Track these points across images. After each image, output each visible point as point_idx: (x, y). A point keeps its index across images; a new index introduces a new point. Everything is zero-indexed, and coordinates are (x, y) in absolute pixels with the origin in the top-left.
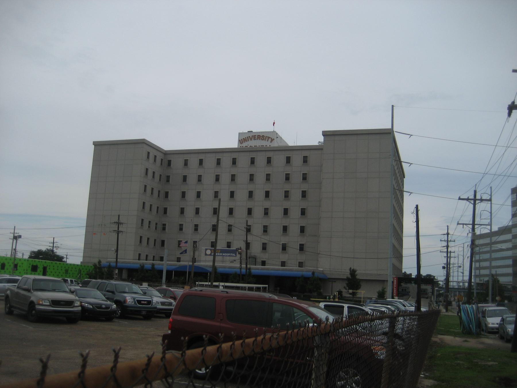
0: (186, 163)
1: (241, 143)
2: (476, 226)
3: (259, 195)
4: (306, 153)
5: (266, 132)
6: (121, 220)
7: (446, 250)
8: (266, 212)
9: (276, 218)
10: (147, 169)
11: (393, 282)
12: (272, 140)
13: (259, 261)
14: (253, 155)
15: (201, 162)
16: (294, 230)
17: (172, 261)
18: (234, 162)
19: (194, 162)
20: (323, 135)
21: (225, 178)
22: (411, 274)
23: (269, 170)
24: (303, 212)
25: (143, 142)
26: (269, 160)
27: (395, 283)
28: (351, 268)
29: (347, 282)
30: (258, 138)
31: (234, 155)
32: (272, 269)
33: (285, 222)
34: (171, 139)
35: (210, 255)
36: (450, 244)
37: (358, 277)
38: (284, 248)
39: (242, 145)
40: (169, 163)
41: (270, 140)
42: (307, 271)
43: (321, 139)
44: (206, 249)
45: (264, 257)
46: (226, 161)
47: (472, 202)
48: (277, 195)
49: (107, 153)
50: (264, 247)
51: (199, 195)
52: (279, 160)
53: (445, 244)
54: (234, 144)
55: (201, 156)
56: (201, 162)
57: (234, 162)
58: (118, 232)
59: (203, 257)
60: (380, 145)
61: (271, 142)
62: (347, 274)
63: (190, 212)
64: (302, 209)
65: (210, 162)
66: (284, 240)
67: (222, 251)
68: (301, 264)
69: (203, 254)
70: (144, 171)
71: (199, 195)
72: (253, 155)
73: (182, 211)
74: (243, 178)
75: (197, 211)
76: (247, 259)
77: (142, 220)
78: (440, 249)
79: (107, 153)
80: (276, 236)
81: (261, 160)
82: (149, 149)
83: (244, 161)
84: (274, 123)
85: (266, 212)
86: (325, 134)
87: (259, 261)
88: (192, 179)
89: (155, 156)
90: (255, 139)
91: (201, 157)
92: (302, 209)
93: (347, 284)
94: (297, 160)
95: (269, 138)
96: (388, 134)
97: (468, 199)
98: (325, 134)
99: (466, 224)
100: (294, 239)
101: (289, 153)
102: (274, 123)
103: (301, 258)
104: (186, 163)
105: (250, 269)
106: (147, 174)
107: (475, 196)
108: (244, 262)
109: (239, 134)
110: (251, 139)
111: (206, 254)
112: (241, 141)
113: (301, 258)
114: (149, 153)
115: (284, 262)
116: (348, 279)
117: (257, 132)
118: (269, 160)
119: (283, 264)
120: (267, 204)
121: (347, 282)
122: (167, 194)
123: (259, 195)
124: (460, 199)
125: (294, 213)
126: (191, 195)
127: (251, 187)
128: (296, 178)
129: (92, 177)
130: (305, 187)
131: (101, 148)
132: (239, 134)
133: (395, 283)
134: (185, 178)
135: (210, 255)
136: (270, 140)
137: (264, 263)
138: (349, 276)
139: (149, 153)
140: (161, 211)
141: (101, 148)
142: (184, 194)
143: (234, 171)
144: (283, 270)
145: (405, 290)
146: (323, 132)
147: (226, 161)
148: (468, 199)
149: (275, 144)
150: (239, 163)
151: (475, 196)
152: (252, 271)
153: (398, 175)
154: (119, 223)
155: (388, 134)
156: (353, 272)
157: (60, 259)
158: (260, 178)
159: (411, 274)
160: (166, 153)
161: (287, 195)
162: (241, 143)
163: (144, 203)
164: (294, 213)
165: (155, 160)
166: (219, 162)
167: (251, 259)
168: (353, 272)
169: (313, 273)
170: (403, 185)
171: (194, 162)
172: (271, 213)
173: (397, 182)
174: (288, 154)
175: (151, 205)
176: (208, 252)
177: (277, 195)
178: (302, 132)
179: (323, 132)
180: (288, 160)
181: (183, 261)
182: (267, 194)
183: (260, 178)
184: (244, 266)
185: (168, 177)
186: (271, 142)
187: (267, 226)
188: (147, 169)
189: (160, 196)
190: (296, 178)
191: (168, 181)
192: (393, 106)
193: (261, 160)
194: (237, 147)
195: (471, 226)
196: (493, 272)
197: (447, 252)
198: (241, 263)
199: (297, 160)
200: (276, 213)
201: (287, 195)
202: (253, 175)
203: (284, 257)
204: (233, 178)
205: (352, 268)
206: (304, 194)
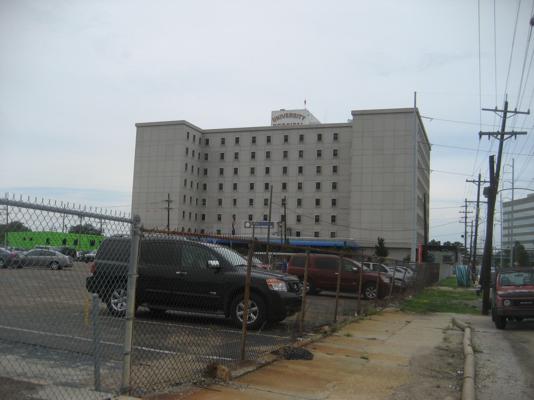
0: (223, 142)
1: (274, 121)
2: (480, 204)
3: (293, 170)
4: (336, 131)
5: (298, 110)
6: (172, 198)
7: (464, 221)
8: (300, 186)
9: (309, 193)
10: (187, 149)
11: (417, 250)
12: (304, 118)
13: (294, 232)
14: (286, 133)
15: (237, 140)
16: (326, 203)
17: (310, 236)
18: (269, 140)
19: (230, 140)
20: (353, 115)
21: (261, 155)
22: (439, 242)
23: (301, 147)
24: (334, 186)
25: (183, 124)
26: (302, 138)
27: (420, 251)
28: (379, 238)
29: (376, 250)
30: (290, 116)
31: (269, 134)
32: (308, 240)
33: (318, 196)
34: (209, 118)
35: (250, 227)
36: (468, 215)
37: (385, 246)
38: (317, 219)
39: (275, 123)
40: (207, 142)
41: (302, 118)
42: (339, 240)
43: (351, 118)
44: (246, 222)
45: (298, 228)
46: (261, 139)
47: (477, 183)
48: (310, 170)
49: (149, 134)
50: (299, 219)
51: (236, 171)
52: (311, 137)
53: (464, 215)
54: (268, 123)
55: (237, 134)
56: (237, 140)
57: (269, 140)
58: (169, 209)
59: (243, 230)
60: (409, 120)
61: (303, 120)
62: (376, 243)
63: (228, 187)
64: (333, 183)
65: (246, 140)
66: (317, 212)
67: (261, 224)
68: (317, 234)
69: (243, 227)
70: (184, 151)
71: (236, 171)
72: (286, 133)
73: (221, 187)
74: (277, 155)
75: (235, 187)
76: (285, 231)
77: (185, 196)
78: (459, 220)
79: (149, 134)
80: (309, 210)
81: (294, 137)
82: (189, 130)
83: (277, 139)
84: (305, 101)
85: (300, 186)
86: (354, 113)
87: (294, 232)
88: (229, 156)
89: (194, 136)
90: (287, 117)
91: (237, 135)
92: (333, 183)
93: (376, 253)
94: (328, 137)
95: (301, 115)
96: (414, 113)
97: (474, 181)
98: (354, 113)
99: (472, 202)
100: (326, 211)
101: (320, 131)
102: (305, 101)
103: (333, 229)
104: (223, 142)
105: (288, 239)
106: (187, 153)
107: (480, 178)
108: (283, 233)
109: (272, 112)
110: (284, 117)
111: (245, 227)
112: (274, 119)
113: (333, 229)
114: (188, 133)
115: (299, 232)
116: (376, 247)
117: (289, 111)
118: (302, 138)
119: (317, 234)
120: (301, 179)
121: (376, 250)
122: (206, 171)
123: (293, 170)
124: (467, 181)
125: (327, 187)
126: (229, 171)
127: (285, 164)
128: (328, 154)
129: (136, 157)
130: (335, 162)
131: (142, 128)
132: (272, 112)
133: (420, 251)
134: (222, 156)
135: (250, 227)
136: (302, 118)
137: (298, 234)
138: (378, 245)
139: (188, 133)
140: (201, 187)
141: (142, 128)
142: (222, 171)
143: (268, 148)
144: (317, 240)
145: (431, 257)
146: (352, 111)
147: (261, 139)
148: (474, 181)
149: (306, 122)
150: (273, 140)
151: (480, 178)
152: (290, 241)
153: (423, 149)
154: (169, 201)
155: (414, 113)
156: (381, 241)
157: (27, 230)
158: (294, 155)
159: (439, 242)
160: (204, 133)
161: (319, 170)
162: (274, 121)
163: (185, 180)
164: (327, 187)
165: (194, 140)
166: (254, 140)
167: (288, 231)
168: (381, 241)
169: (345, 243)
170: (429, 158)
171: (230, 140)
172: (305, 187)
173: (423, 157)
174: (320, 132)
175: (192, 182)
176: (248, 225)
177: (310, 170)
178: (332, 110)
179: (352, 111)
180: (320, 137)
181: (339, 237)
182: (300, 170)
183: (294, 155)
184: (284, 237)
185: (207, 155)
186: (303, 120)
187: (335, 216)
188: (187, 149)
189: (200, 173)
190: (328, 154)
191: (206, 158)
192: (415, 93)
193: (294, 137)
194: (270, 126)
195: (476, 203)
196: (518, 239)
197: (466, 222)
198: (282, 235)
199: (328, 137)
200: (309, 187)
201: (319, 170)
202: (287, 152)
203: (317, 228)
204: (268, 155)
205: (380, 238)
206: (335, 169)
